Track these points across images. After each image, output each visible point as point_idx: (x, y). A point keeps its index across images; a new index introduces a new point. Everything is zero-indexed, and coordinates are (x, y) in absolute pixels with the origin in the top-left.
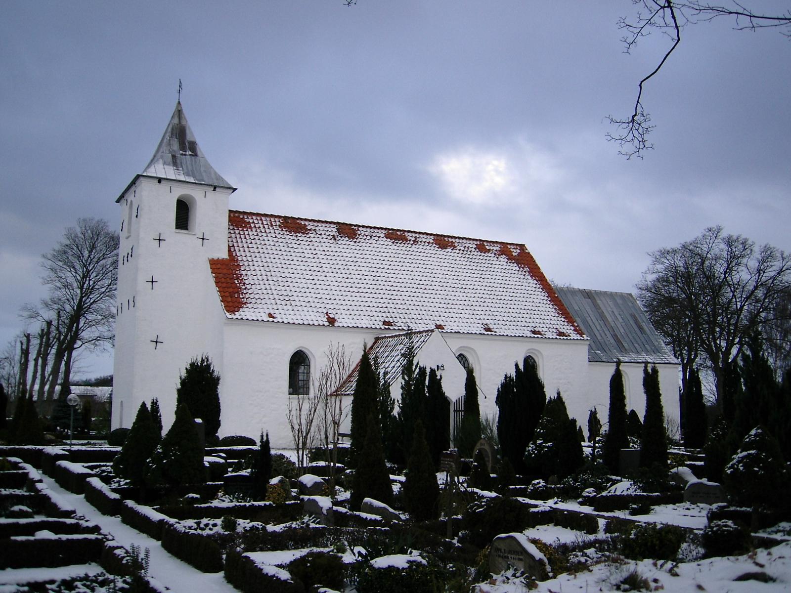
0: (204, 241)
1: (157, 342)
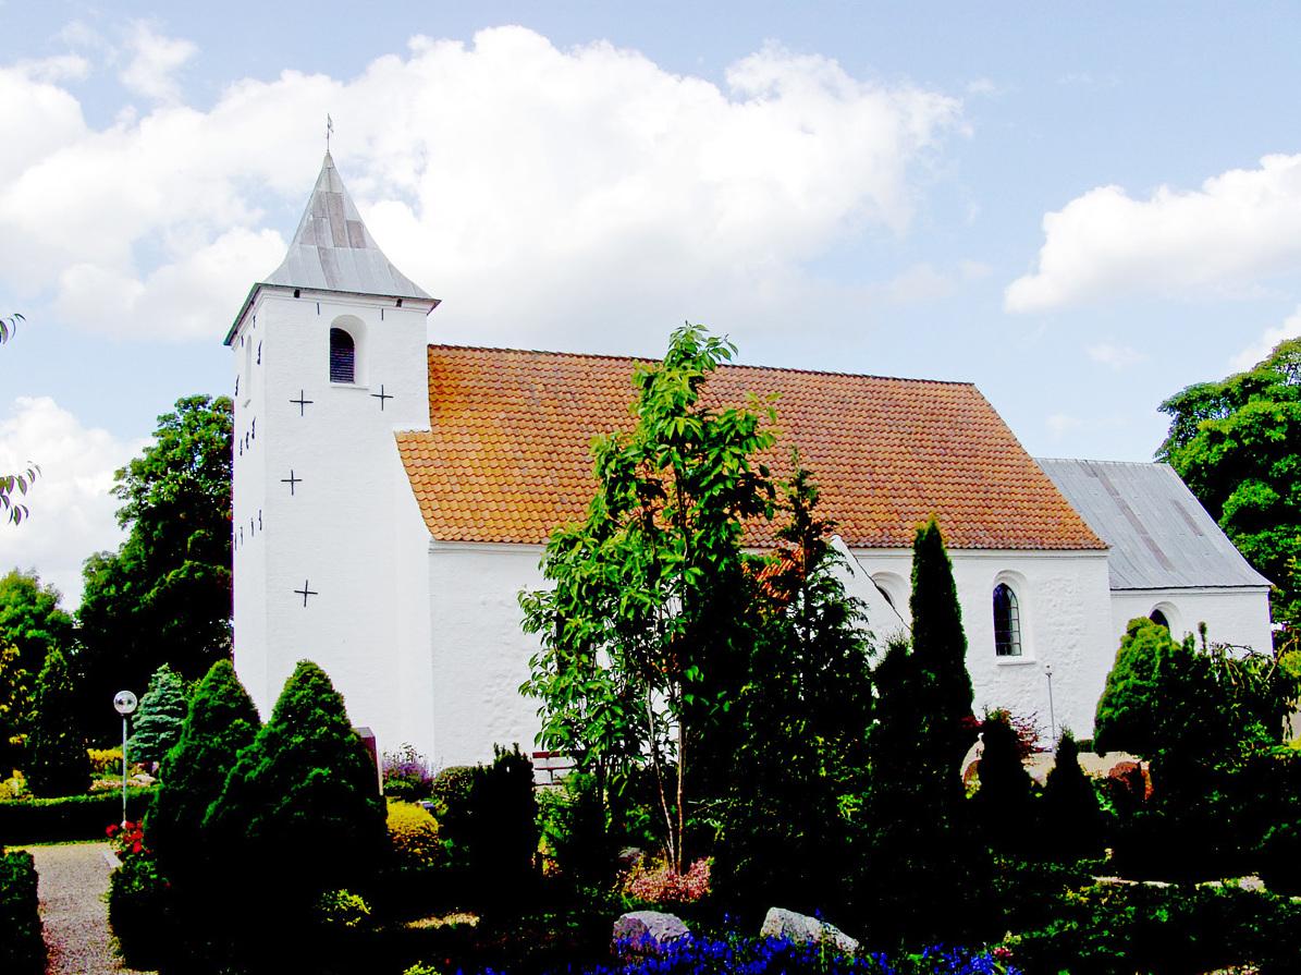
0: (380, 399)
1: (306, 593)
